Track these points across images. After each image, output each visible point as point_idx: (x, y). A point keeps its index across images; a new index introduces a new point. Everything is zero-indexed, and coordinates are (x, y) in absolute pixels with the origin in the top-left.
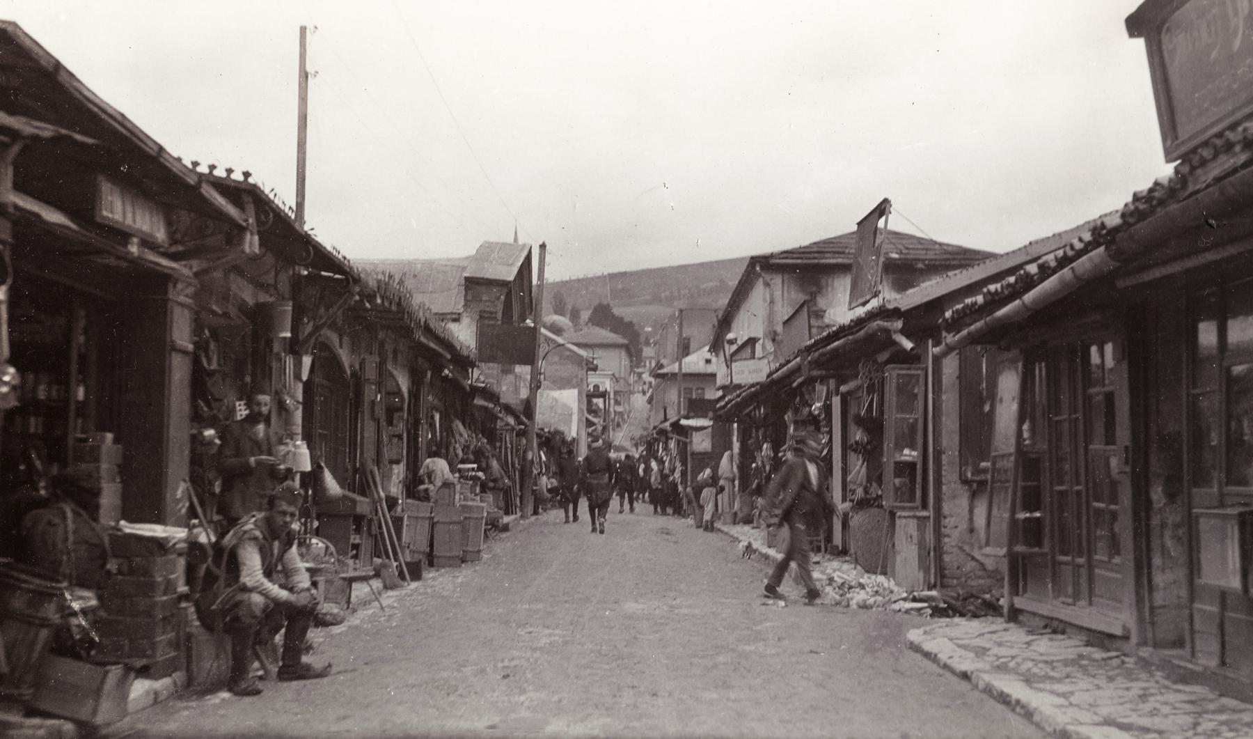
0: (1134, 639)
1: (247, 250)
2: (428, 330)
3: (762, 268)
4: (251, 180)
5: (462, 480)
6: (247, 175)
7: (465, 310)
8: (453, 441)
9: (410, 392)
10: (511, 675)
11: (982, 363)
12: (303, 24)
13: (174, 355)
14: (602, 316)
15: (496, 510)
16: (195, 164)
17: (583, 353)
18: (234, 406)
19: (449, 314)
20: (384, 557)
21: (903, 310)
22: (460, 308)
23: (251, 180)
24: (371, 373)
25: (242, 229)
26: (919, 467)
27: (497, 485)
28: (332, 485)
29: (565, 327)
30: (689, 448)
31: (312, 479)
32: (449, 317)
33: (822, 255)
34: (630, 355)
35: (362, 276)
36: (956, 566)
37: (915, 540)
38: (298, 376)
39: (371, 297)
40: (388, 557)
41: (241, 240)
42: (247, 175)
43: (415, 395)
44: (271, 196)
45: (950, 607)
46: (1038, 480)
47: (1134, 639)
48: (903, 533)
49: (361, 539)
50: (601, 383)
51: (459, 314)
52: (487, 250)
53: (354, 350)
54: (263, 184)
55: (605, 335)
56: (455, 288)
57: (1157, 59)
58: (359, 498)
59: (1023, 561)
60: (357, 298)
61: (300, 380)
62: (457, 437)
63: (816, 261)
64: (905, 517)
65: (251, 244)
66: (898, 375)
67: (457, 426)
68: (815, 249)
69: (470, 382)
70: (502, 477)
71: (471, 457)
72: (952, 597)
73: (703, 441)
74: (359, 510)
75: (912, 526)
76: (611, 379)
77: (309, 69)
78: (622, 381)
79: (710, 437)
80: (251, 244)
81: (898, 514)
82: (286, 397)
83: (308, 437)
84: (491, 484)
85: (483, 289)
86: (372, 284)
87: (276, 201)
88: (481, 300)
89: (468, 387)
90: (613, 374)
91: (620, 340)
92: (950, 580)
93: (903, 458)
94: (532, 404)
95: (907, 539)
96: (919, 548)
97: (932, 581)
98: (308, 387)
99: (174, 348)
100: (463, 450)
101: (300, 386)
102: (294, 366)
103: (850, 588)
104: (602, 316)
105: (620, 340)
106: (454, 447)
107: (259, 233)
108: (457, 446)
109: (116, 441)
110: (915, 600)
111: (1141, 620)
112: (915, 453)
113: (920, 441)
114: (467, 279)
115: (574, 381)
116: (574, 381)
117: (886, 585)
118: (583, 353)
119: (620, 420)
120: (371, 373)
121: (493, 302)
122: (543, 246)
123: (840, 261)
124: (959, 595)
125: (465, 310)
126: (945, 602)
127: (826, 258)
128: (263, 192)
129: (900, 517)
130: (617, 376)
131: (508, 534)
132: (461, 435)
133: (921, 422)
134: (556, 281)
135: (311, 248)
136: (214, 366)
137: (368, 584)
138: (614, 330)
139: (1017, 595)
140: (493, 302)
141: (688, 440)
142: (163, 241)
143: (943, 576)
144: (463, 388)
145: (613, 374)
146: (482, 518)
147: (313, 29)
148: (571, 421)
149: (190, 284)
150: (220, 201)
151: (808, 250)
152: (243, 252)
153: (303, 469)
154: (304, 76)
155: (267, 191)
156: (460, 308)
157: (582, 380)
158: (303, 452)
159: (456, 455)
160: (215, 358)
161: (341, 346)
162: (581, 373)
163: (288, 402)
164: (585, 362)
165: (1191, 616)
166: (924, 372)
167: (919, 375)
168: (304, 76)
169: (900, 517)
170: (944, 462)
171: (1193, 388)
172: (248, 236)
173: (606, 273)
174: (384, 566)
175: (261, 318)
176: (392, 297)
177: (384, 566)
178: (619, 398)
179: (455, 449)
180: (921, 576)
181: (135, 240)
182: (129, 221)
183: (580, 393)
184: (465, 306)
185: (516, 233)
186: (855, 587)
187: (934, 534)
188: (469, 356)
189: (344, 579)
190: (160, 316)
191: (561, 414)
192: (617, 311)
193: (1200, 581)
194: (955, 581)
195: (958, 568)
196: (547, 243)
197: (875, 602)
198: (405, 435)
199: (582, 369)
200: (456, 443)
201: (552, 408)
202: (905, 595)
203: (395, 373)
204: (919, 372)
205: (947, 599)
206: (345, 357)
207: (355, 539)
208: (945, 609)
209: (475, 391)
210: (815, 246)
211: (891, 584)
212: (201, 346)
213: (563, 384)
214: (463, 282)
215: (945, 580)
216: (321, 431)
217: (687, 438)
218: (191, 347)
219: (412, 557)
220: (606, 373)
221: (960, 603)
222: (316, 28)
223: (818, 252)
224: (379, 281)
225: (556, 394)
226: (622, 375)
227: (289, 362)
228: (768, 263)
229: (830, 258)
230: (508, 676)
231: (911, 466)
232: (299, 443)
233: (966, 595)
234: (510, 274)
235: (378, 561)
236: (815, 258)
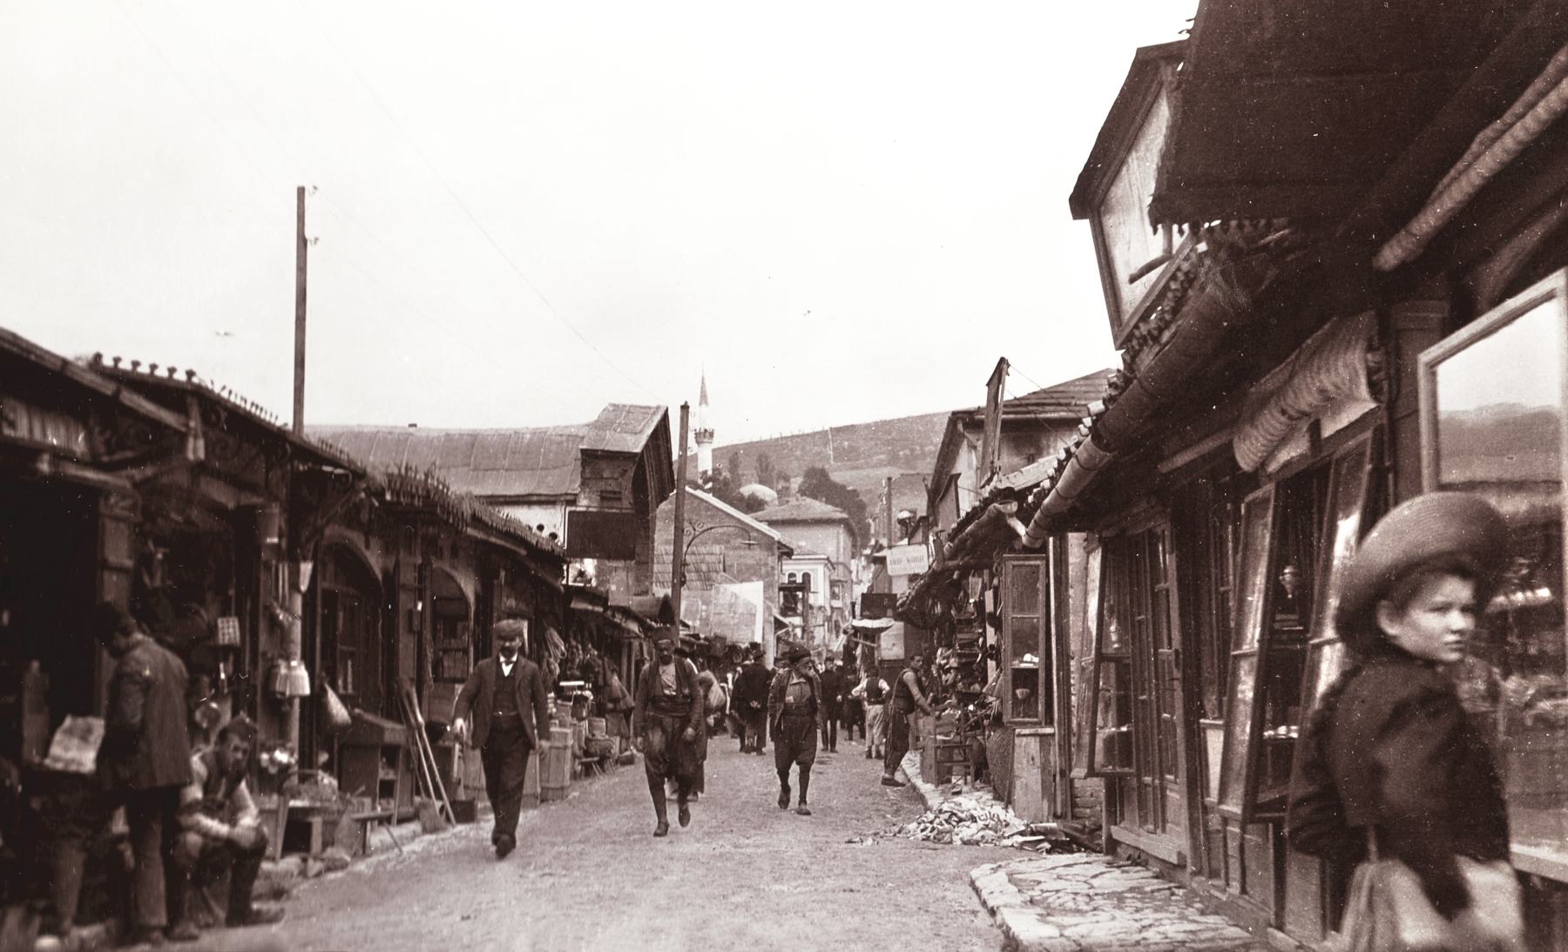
0: (1191, 868)
1: (191, 456)
2: (477, 521)
3: (966, 426)
4: (195, 380)
5: (559, 702)
6: (190, 374)
7: (583, 491)
8: (547, 654)
9: (477, 596)
10: (472, 916)
11: (344, 624)
12: (301, 184)
13: (106, 575)
14: (819, 485)
15: (607, 737)
16: (136, 364)
17: (776, 534)
18: (216, 626)
19: (561, 495)
20: (423, 795)
21: (1016, 489)
22: (575, 487)
23: (195, 380)
24: (408, 576)
25: (183, 437)
26: (1042, 675)
27: (618, 708)
28: (338, 710)
29: (767, 499)
30: (876, 655)
31: (314, 705)
32: (562, 499)
33: (1040, 409)
34: (851, 532)
35: (369, 470)
36: (1089, 793)
37: (1038, 760)
38: (294, 586)
39: (380, 494)
40: (429, 795)
41: (182, 448)
42: (190, 374)
43: (484, 598)
44: (225, 394)
45: (1074, 840)
46: (516, 707)
47: (1191, 868)
48: (1023, 754)
49: (396, 774)
50: (812, 570)
51: (576, 495)
52: (617, 415)
53: (388, 549)
54: (212, 383)
55: (820, 508)
56: (571, 464)
57: (1100, 240)
58: (388, 725)
59: (1120, 783)
60: (363, 495)
61: (299, 591)
62: (552, 649)
63: (1033, 416)
64: (1024, 735)
65: (195, 451)
66: (1014, 566)
67: (551, 635)
68: (1033, 401)
69: (564, 582)
70: (624, 696)
71: (577, 673)
72: (1076, 830)
73: (894, 645)
74: (388, 738)
75: (1033, 745)
76: (826, 565)
77: (308, 234)
78: (841, 568)
79: (902, 641)
80: (195, 451)
81: (1017, 731)
82: (278, 611)
83: (308, 661)
84: (610, 706)
85: (603, 464)
86: (381, 479)
87: (232, 399)
88: (602, 478)
89: (562, 588)
90: (828, 559)
91: (839, 514)
92: (1081, 810)
93: (1023, 665)
94: (674, 604)
95: (1028, 762)
96: (1043, 772)
97: (1059, 811)
98: (309, 598)
99: (105, 566)
100: (560, 665)
101: (298, 602)
102: (290, 574)
103: (961, 820)
104: (819, 485)
105: (839, 514)
106: (548, 662)
107: (205, 435)
108: (552, 660)
109: (42, 668)
110: (1033, 833)
111: (1195, 848)
112: (1036, 660)
113: (1042, 647)
114: (583, 451)
115: (763, 570)
116: (763, 570)
117: (1002, 817)
118: (776, 534)
119: (839, 618)
120: (408, 576)
121: (616, 479)
122: (685, 408)
123: (1063, 414)
124: (1085, 826)
125: (583, 491)
126: (1067, 835)
127: (1046, 412)
128: (212, 392)
129: (1019, 735)
130: (833, 560)
131: (632, 767)
132: (557, 647)
133: (1042, 623)
134: (764, 438)
135: (288, 446)
136: (158, 583)
137: (388, 830)
138: (829, 501)
139: (1115, 824)
140: (616, 479)
141: (875, 645)
142: (82, 454)
143: (1074, 805)
144: (558, 590)
145: (828, 559)
146: (565, 748)
147: (312, 189)
148: (754, 624)
149: (124, 497)
150: (148, 407)
151: (1023, 402)
152: (186, 459)
153: (301, 692)
154: (302, 242)
155: (217, 390)
156: (575, 487)
157: (773, 568)
158: (302, 673)
159: (551, 672)
160: (159, 575)
161: (367, 546)
162: (772, 561)
163: (281, 617)
164: (776, 546)
165: (1225, 838)
166: (1044, 562)
167: (1038, 566)
168: (302, 242)
169: (1019, 735)
170: (1072, 669)
171: (1222, 585)
172: (191, 441)
173: (827, 428)
174: (424, 806)
175: (246, 523)
176: (414, 490)
177: (424, 806)
178: (836, 590)
179: (549, 664)
180: (1045, 805)
181: (46, 457)
182: (38, 435)
183: (767, 587)
184: (583, 484)
185: (703, 379)
186: (965, 821)
187: (1060, 755)
188: (553, 550)
189: (357, 820)
190: (91, 535)
191: (742, 614)
192: (837, 477)
193: (1208, 799)
194: (1088, 811)
195: (1092, 795)
196: (689, 404)
197: (983, 837)
198: (472, 649)
199: (773, 554)
200: (550, 656)
201: (731, 606)
202: (1023, 828)
203: (455, 574)
204: (1038, 562)
205: (1068, 831)
206: (375, 559)
207: (384, 774)
208: (1069, 843)
209: (572, 592)
210: (1033, 396)
211: (1010, 816)
212: (144, 561)
213: (743, 575)
214: (580, 455)
215: (1077, 810)
216: (344, 648)
217: (873, 642)
218: (129, 563)
219: (466, 795)
220: (818, 557)
221: (1085, 837)
222: (315, 188)
223: (1037, 405)
224: (390, 476)
225: (736, 588)
226: (841, 560)
227: (284, 572)
228: (973, 419)
229: (1051, 412)
230: (468, 917)
231: (1033, 673)
232: (294, 663)
233: (1093, 827)
234: (636, 444)
235: (417, 799)
236: (1029, 413)
